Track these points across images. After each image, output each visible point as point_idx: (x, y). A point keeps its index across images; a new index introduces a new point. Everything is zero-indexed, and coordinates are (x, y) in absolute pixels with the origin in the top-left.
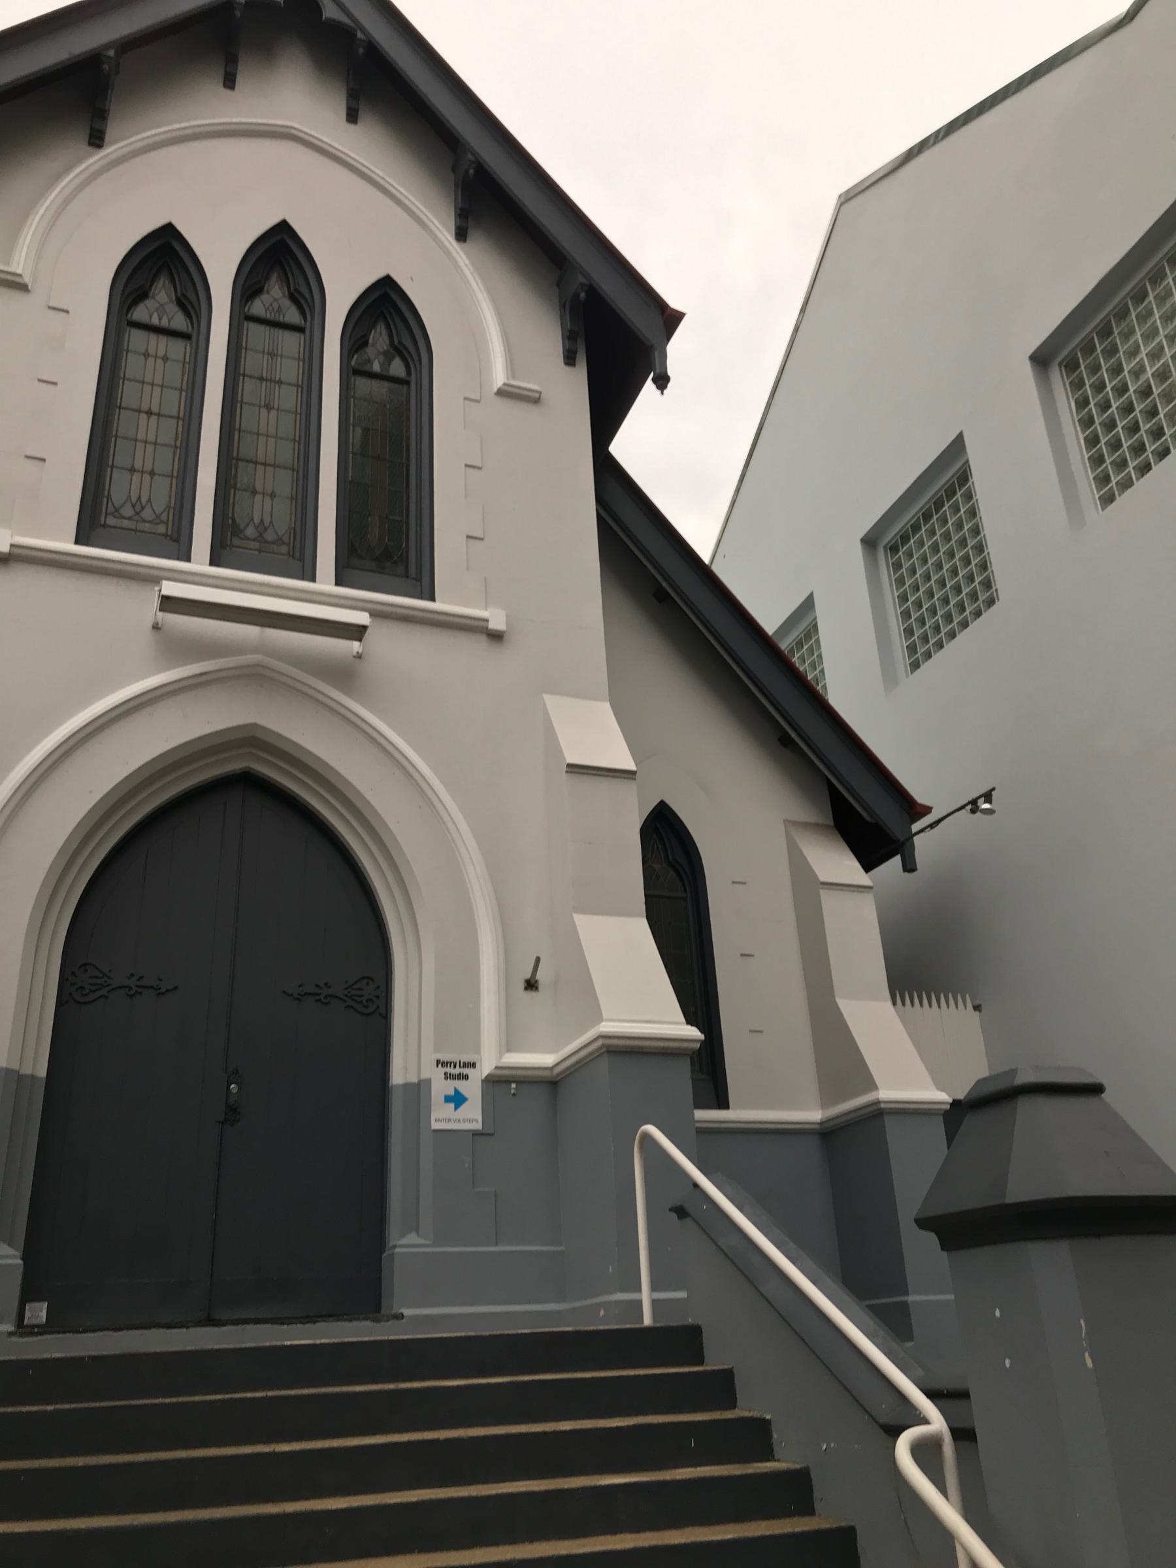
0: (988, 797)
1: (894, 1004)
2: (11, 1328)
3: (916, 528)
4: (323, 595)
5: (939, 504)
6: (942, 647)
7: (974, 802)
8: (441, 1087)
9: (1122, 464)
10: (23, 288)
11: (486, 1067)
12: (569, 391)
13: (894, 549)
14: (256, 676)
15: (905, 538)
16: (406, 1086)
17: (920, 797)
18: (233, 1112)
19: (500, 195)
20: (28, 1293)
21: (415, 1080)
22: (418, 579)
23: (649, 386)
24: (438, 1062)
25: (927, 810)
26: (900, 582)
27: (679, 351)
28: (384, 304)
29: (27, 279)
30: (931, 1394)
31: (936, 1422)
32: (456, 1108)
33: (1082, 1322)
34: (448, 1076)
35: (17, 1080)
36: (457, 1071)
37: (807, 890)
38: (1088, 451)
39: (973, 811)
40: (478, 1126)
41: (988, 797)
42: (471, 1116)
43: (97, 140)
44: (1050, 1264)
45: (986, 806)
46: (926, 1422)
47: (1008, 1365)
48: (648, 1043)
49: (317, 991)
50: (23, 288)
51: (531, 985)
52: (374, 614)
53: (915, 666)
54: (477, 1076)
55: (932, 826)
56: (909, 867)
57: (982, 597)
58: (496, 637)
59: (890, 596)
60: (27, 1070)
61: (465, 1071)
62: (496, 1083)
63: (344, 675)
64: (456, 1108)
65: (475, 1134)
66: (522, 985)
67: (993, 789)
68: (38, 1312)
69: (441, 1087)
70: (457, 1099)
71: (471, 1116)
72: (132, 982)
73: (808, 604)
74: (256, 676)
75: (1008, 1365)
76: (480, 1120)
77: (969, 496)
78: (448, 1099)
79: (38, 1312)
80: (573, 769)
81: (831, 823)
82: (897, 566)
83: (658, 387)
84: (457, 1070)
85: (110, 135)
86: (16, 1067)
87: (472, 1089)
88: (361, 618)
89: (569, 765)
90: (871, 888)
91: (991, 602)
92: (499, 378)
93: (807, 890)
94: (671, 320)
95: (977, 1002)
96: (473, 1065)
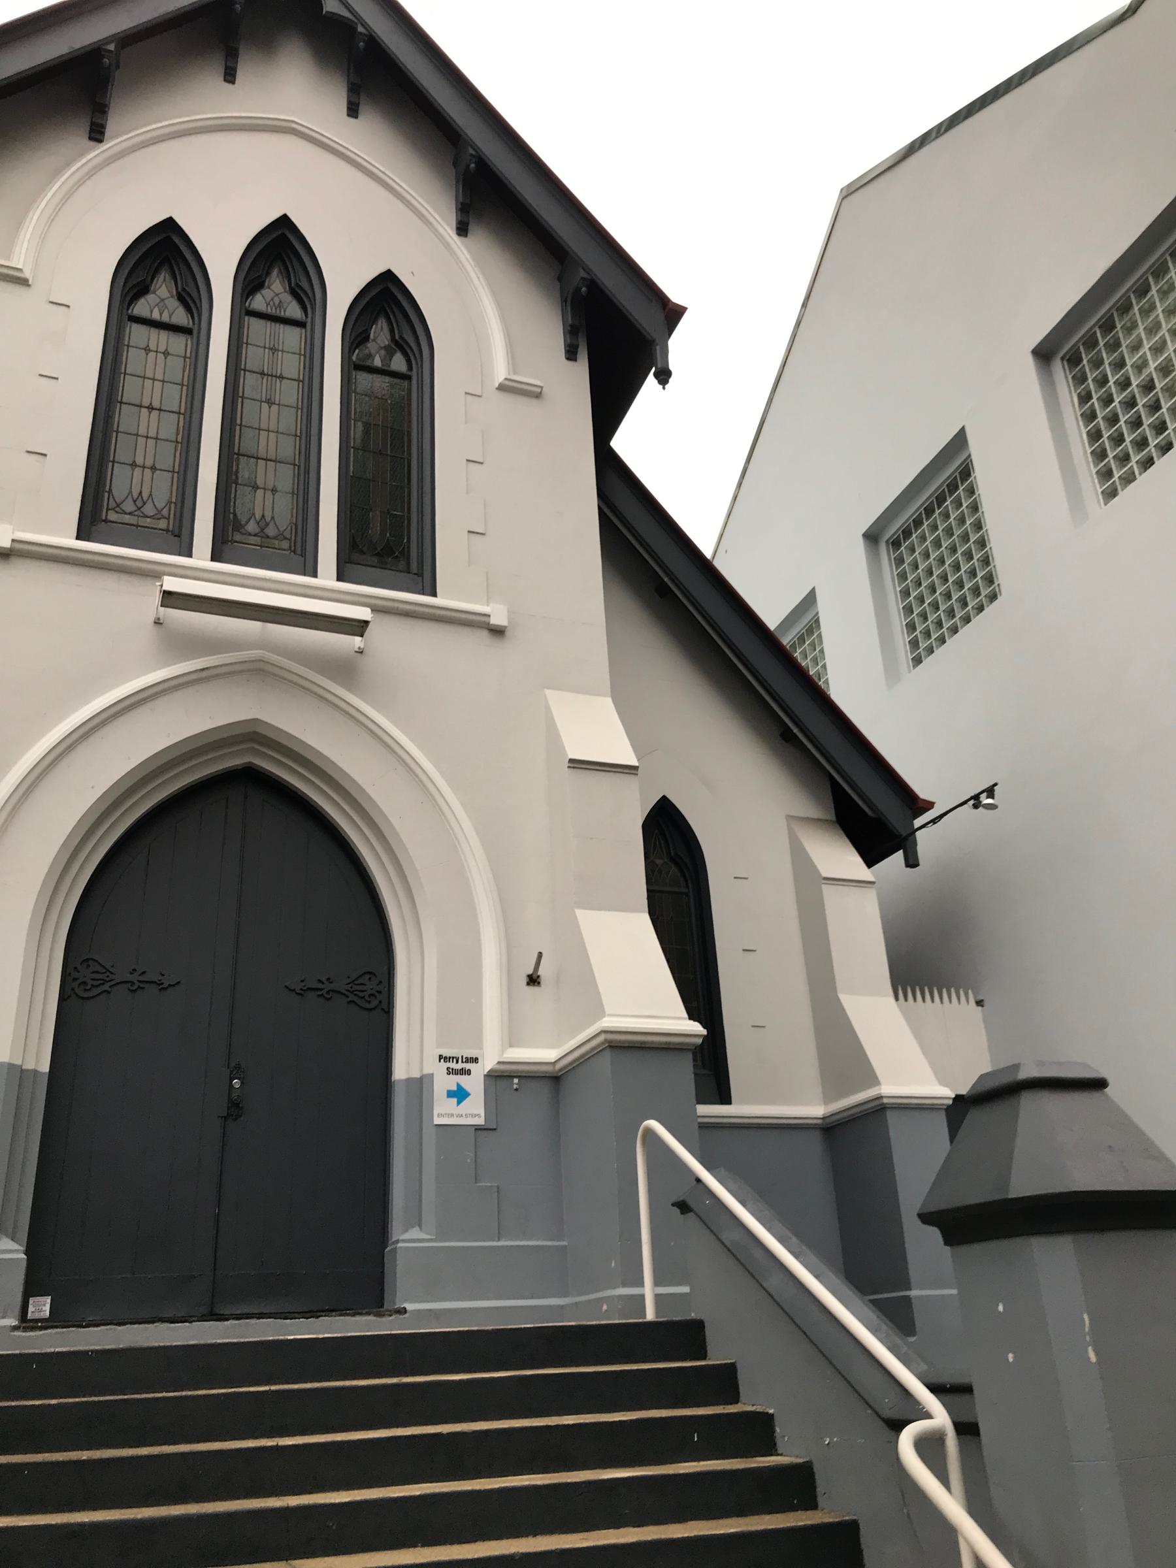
0: (990, 791)
1: (897, 999)
2: (15, 1323)
3: (918, 523)
4: (325, 590)
5: (941, 500)
6: (944, 642)
7: (976, 797)
8: (443, 1082)
9: (1124, 459)
10: (24, 282)
11: (488, 1063)
12: (572, 384)
13: (896, 544)
14: (259, 672)
15: (907, 533)
16: (409, 1081)
17: (923, 793)
18: (235, 1108)
19: (501, 189)
20: (32, 1288)
21: (416, 1074)
22: (420, 574)
23: (651, 381)
24: (441, 1057)
25: (929, 805)
26: (903, 576)
27: (680, 347)
28: (385, 299)
29: (27, 274)
30: (935, 1389)
31: (939, 1416)
32: (459, 1103)
33: (1086, 1316)
34: (450, 1071)
35: (19, 1075)
36: (460, 1066)
37: (810, 885)
38: (1091, 445)
39: (976, 806)
40: (481, 1121)
41: (990, 791)
42: (473, 1111)
43: (97, 134)
44: (1054, 1260)
45: (990, 801)
46: (928, 1416)
47: (1011, 1360)
48: (845, 1114)
49: (320, 986)
50: (24, 282)
51: (533, 980)
52: (375, 610)
53: (917, 661)
54: (479, 1071)
55: (934, 821)
56: (912, 862)
57: (985, 592)
58: (498, 632)
59: (892, 590)
60: (29, 1065)
61: (468, 1066)
62: (498, 1078)
63: (345, 670)
64: (459, 1103)
65: (478, 1129)
66: (525, 980)
67: (996, 784)
68: (41, 1307)
69: (443, 1082)
70: (460, 1094)
71: (473, 1111)
72: (134, 978)
73: (810, 599)
74: (259, 672)
75: (1011, 1360)
76: (483, 1115)
77: (971, 491)
78: (450, 1094)
79: (41, 1307)
80: (575, 764)
81: (834, 818)
82: (900, 561)
83: (660, 382)
84: (459, 1065)
85: (112, 124)
86: (19, 1062)
87: (475, 1083)
88: (363, 613)
89: (571, 761)
90: (873, 883)
91: (993, 597)
92: (501, 372)
93: (810, 885)
94: (672, 314)
95: (980, 998)
96: (476, 1060)
